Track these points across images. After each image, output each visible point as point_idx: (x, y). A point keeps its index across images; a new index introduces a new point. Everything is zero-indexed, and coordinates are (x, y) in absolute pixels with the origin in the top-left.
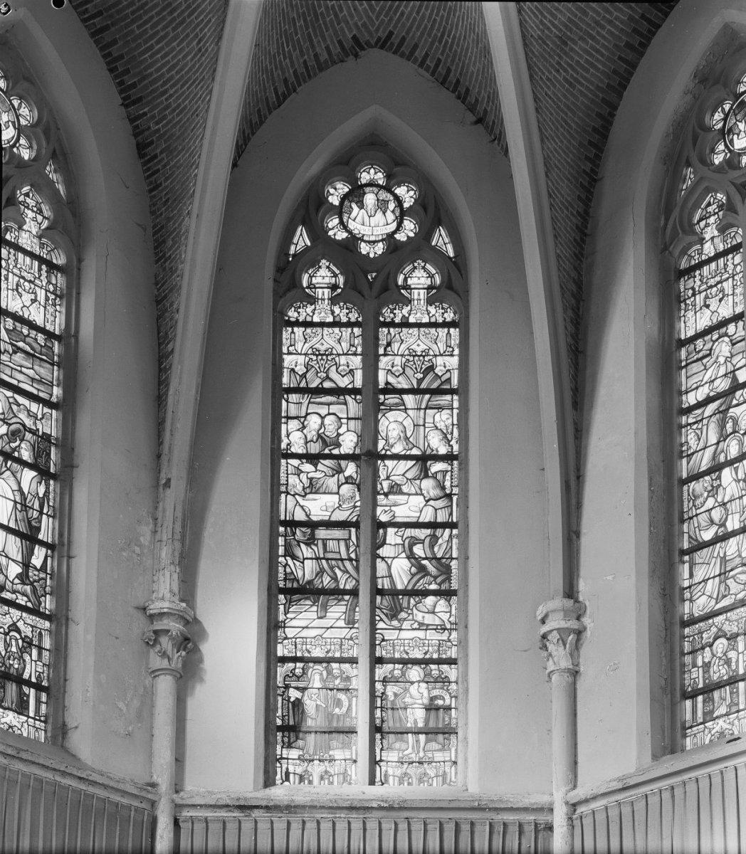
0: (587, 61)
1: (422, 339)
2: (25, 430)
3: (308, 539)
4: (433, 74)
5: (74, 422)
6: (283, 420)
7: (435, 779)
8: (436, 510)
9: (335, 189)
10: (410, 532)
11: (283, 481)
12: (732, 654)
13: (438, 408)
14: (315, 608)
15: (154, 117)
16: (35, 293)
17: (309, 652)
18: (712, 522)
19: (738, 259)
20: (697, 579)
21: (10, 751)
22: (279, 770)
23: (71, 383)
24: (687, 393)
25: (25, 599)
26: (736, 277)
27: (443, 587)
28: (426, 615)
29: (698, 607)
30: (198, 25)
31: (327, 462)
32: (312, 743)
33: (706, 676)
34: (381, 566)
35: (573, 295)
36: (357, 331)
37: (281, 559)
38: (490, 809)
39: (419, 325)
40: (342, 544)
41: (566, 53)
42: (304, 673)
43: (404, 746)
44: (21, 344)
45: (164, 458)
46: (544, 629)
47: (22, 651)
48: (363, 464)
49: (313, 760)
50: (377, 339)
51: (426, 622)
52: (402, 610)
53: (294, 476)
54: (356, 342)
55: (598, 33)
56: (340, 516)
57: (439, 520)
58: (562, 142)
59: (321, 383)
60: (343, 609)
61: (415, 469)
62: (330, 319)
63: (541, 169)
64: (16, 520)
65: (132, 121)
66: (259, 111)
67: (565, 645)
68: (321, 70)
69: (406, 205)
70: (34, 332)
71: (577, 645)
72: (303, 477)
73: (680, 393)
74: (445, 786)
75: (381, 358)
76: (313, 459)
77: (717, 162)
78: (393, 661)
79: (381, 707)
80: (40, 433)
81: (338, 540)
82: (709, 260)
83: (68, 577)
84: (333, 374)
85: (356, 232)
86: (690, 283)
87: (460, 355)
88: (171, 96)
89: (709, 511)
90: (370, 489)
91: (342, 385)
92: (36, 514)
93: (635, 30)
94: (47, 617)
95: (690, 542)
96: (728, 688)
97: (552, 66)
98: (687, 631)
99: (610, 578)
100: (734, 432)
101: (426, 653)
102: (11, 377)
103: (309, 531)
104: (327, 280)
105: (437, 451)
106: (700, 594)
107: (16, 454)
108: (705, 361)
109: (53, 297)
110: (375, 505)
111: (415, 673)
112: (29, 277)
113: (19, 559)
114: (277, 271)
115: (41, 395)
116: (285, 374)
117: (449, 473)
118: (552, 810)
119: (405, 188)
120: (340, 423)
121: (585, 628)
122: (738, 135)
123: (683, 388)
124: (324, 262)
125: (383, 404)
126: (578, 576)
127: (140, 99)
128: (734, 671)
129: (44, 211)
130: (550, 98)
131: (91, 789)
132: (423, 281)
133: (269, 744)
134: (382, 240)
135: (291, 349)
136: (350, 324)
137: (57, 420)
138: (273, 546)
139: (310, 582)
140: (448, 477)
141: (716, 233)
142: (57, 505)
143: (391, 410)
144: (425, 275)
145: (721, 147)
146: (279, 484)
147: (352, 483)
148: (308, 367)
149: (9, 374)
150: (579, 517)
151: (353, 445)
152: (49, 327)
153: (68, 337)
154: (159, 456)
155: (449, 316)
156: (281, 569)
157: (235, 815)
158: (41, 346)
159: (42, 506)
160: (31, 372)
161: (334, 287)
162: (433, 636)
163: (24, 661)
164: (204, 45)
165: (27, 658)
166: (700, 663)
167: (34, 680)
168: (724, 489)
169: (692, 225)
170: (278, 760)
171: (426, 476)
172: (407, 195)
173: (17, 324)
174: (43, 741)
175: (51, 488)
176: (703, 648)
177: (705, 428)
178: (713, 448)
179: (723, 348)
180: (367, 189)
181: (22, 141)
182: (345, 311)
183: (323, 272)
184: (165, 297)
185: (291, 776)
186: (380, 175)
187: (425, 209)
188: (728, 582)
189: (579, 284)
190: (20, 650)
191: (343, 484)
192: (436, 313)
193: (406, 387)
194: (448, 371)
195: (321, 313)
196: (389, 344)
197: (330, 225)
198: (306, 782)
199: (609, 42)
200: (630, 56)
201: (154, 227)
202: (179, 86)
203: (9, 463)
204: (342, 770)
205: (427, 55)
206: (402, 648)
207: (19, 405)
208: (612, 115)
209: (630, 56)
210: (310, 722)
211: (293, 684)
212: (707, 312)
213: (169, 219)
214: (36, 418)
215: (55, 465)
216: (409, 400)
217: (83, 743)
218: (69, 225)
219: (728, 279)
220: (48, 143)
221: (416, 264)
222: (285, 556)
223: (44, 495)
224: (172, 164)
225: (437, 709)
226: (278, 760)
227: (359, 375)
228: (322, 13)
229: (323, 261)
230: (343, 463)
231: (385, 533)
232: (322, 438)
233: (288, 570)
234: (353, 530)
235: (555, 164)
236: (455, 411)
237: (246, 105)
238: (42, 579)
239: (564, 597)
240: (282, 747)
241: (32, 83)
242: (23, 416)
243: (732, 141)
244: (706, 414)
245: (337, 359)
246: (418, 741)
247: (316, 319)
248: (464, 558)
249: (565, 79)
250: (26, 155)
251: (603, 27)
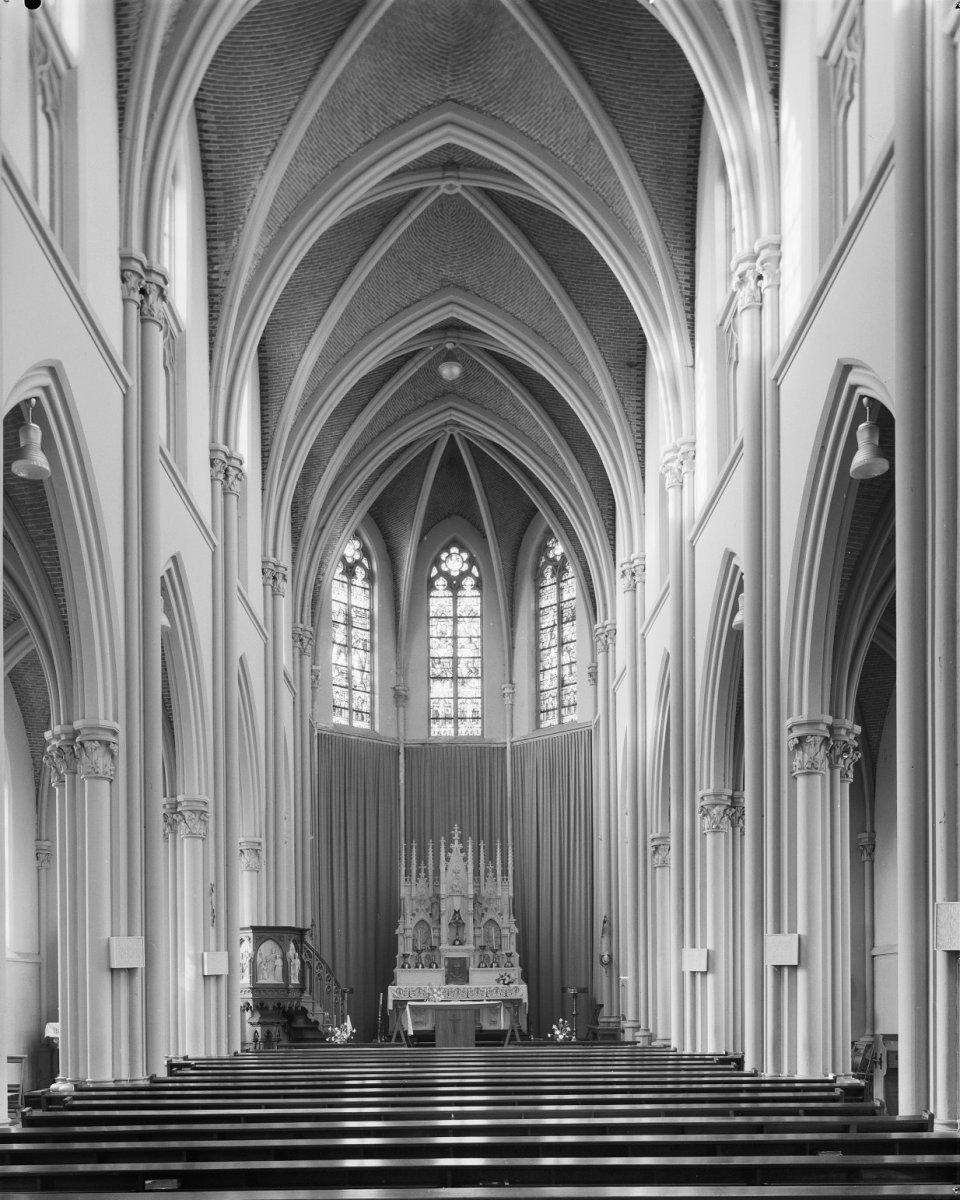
71: (513, 698)
76: (439, 638)
90: (455, 646)
120: (446, 627)
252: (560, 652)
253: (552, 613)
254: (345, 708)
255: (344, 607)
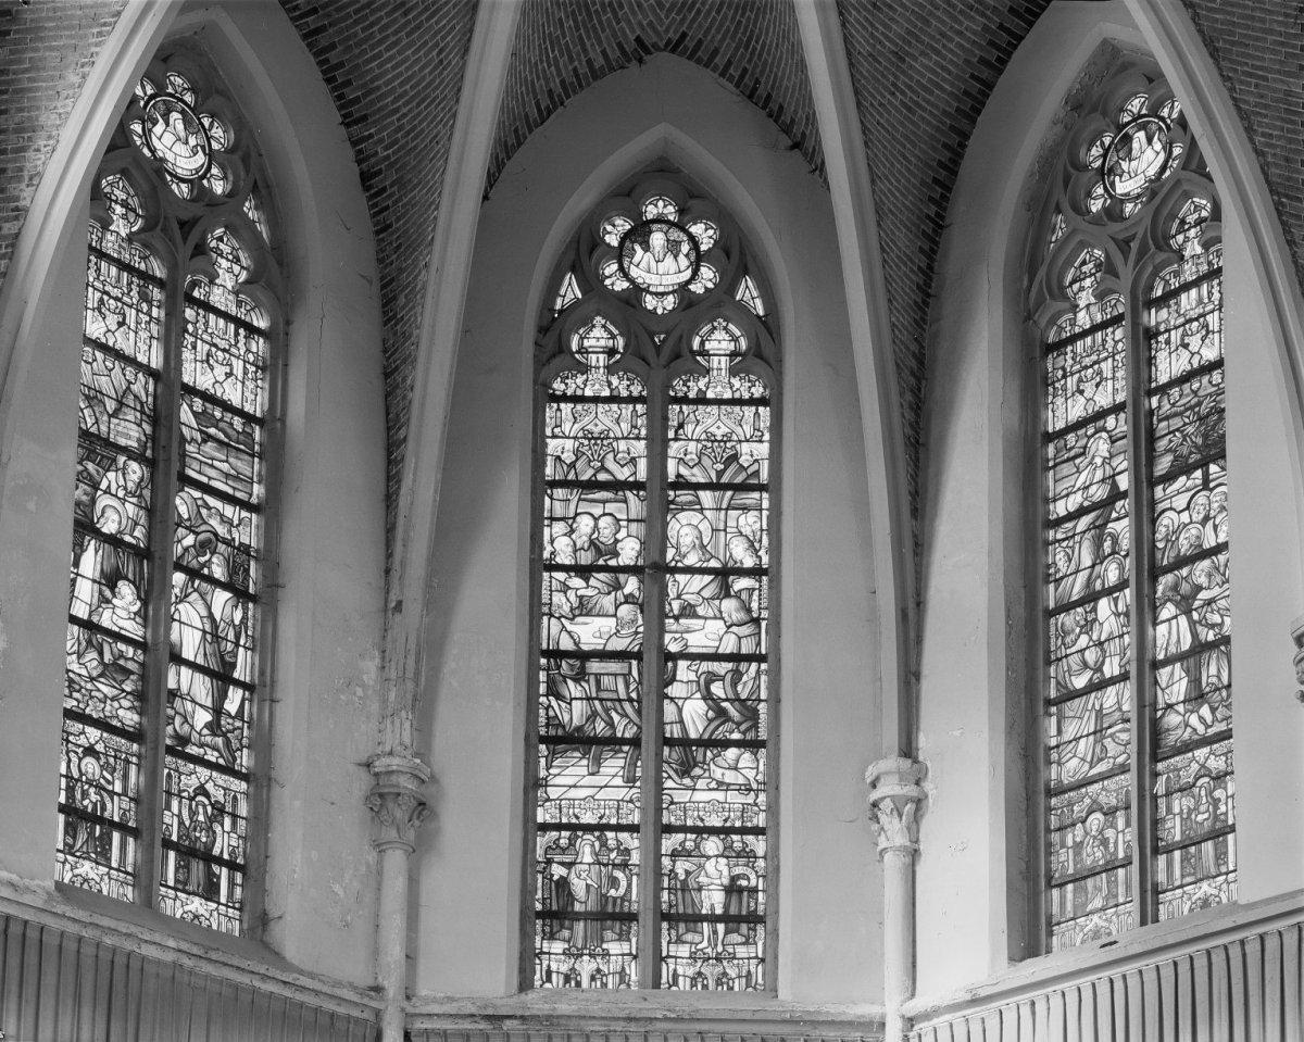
0: (930, 80)
1: (721, 422)
2: (217, 540)
3: (577, 674)
4: (737, 86)
5: (279, 530)
6: (546, 522)
7: (737, 981)
8: (740, 638)
9: (614, 226)
10: (705, 666)
11: (545, 599)
12: (1110, 833)
13: (743, 509)
14: (585, 762)
15: (381, 141)
16: (231, 365)
17: (577, 818)
18: (1085, 665)
19: (1119, 334)
20: (1067, 737)
21: (195, 950)
22: (538, 967)
23: (276, 479)
24: (1055, 501)
25: (216, 754)
26: (1117, 357)
27: (748, 737)
28: (727, 772)
29: (1068, 772)
30: (440, 31)
31: (601, 576)
32: (581, 934)
33: (1078, 859)
34: (669, 710)
35: (913, 373)
36: (640, 408)
37: (542, 699)
38: (805, 1022)
39: (719, 402)
40: (620, 680)
41: (903, 72)
42: (570, 844)
43: (697, 938)
44: (212, 431)
45: (395, 575)
46: (874, 795)
47: (211, 820)
48: (647, 580)
49: (582, 955)
50: (666, 419)
51: (727, 780)
52: (696, 765)
53: (561, 593)
54: (639, 422)
55: (944, 46)
56: (618, 644)
57: (744, 651)
58: (898, 181)
59: (595, 475)
60: (621, 762)
61: (713, 586)
62: (606, 393)
63: (871, 218)
64: (205, 654)
65: (354, 144)
66: (516, 131)
67: (900, 816)
68: (595, 78)
69: (704, 248)
70: (230, 415)
72: (571, 595)
73: (1047, 501)
74: (750, 989)
75: (671, 443)
76: (584, 571)
77: (1094, 209)
78: (684, 829)
79: (669, 889)
80: (237, 544)
81: (615, 675)
82: (1084, 334)
83: (271, 726)
84: (610, 464)
85: (640, 281)
86: (1060, 362)
87: (771, 442)
88: (405, 115)
89: (1082, 651)
90: (655, 610)
91: (621, 477)
92: (230, 647)
93: (991, 43)
94: (191, 391)
95: (1058, 690)
96: (1104, 875)
97: (885, 88)
98: (1054, 801)
99: (957, 733)
100: (1114, 552)
101: (726, 821)
102: (200, 472)
103: (578, 663)
104: (602, 343)
105: (742, 563)
106: (1070, 755)
107: (206, 571)
108: (1077, 461)
109: (254, 369)
110: (662, 630)
111: (712, 845)
112: (223, 344)
113: (209, 704)
114: (539, 332)
115: (239, 495)
116: (548, 463)
117: (757, 592)
118: (884, 1024)
119: (703, 226)
121: (927, 797)
122: (1121, 176)
123: (1051, 495)
124: (599, 320)
125: (672, 502)
126: (918, 728)
127: (364, 118)
128: (1111, 854)
129: (242, 259)
130: (883, 127)
131: (299, 997)
132: (724, 345)
133: (526, 936)
134: (673, 292)
135: (556, 430)
136: (631, 400)
137: (258, 527)
138: (532, 683)
139: (579, 729)
140: (755, 597)
141: (1093, 300)
142: (257, 635)
143: (683, 510)
144: (727, 337)
145: (1100, 191)
146: (541, 604)
147: (633, 603)
148: (578, 454)
149: (197, 468)
150: (919, 654)
151: (634, 554)
152: (248, 408)
153: (273, 420)
154: (387, 571)
155: (758, 391)
156: (542, 712)
157: (481, 1027)
158: (238, 432)
159: (238, 637)
160: (225, 467)
161: (611, 352)
162: (736, 798)
163: (214, 832)
164: (446, 57)
165: (218, 829)
166: (1070, 842)
167: (226, 856)
168: (1101, 624)
169: (1062, 288)
170: (537, 955)
171: (728, 595)
172: (705, 234)
173: (208, 405)
174: (237, 934)
175: (250, 613)
176: (1074, 825)
177: (1077, 546)
178: (1087, 572)
179: (1101, 446)
180: (655, 227)
181: (215, 171)
182: (626, 382)
183: (598, 332)
184: (397, 368)
185: (554, 976)
186: (671, 209)
187: (728, 255)
188: (1106, 742)
189: (920, 359)
190: (210, 818)
191: (621, 604)
192: (742, 388)
193: (702, 481)
194: (756, 461)
195: (595, 386)
196: (681, 426)
197: (607, 272)
198: (573, 983)
199: (957, 56)
200: (985, 74)
201: (382, 279)
202: (414, 104)
203: (197, 582)
204: (619, 969)
205: (729, 63)
206: (696, 814)
207: (209, 508)
208: (962, 146)
209: (985, 74)
210: (578, 907)
211: (557, 858)
212: (1081, 400)
213: (401, 270)
214: (232, 525)
215: (255, 584)
216: (706, 497)
217: (291, 937)
218: (275, 276)
219: (1106, 359)
220: (247, 172)
221: (715, 324)
222: (547, 695)
223: (241, 622)
224: (405, 200)
225: (741, 890)
226: (537, 955)
227: (642, 465)
228: (596, 11)
229: (598, 318)
230: (622, 577)
231: (675, 667)
232: (595, 545)
233: (551, 713)
234: (634, 663)
235: (891, 211)
236: (765, 513)
237: (501, 125)
238: (238, 728)
239: (900, 756)
240: (543, 939)
241: (229, 99)
242: (214, 522)
243: (1113, 184)
244: (1078, 530)
245: (615, 444)
246: (715, 932)
247: (588, 393)
248: (775, 700)
249: (902, 102)
250: (219, 188)
251: (951, 40)
252: (1146, 610)
253: (1101, 446)
254: (122, 827)
255: (142, 386)
